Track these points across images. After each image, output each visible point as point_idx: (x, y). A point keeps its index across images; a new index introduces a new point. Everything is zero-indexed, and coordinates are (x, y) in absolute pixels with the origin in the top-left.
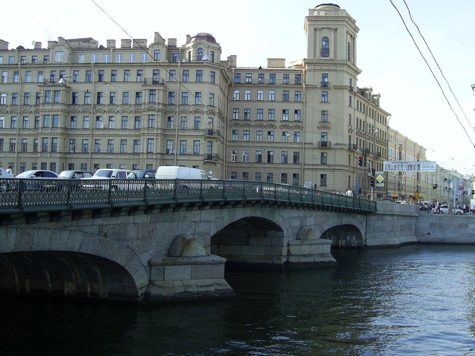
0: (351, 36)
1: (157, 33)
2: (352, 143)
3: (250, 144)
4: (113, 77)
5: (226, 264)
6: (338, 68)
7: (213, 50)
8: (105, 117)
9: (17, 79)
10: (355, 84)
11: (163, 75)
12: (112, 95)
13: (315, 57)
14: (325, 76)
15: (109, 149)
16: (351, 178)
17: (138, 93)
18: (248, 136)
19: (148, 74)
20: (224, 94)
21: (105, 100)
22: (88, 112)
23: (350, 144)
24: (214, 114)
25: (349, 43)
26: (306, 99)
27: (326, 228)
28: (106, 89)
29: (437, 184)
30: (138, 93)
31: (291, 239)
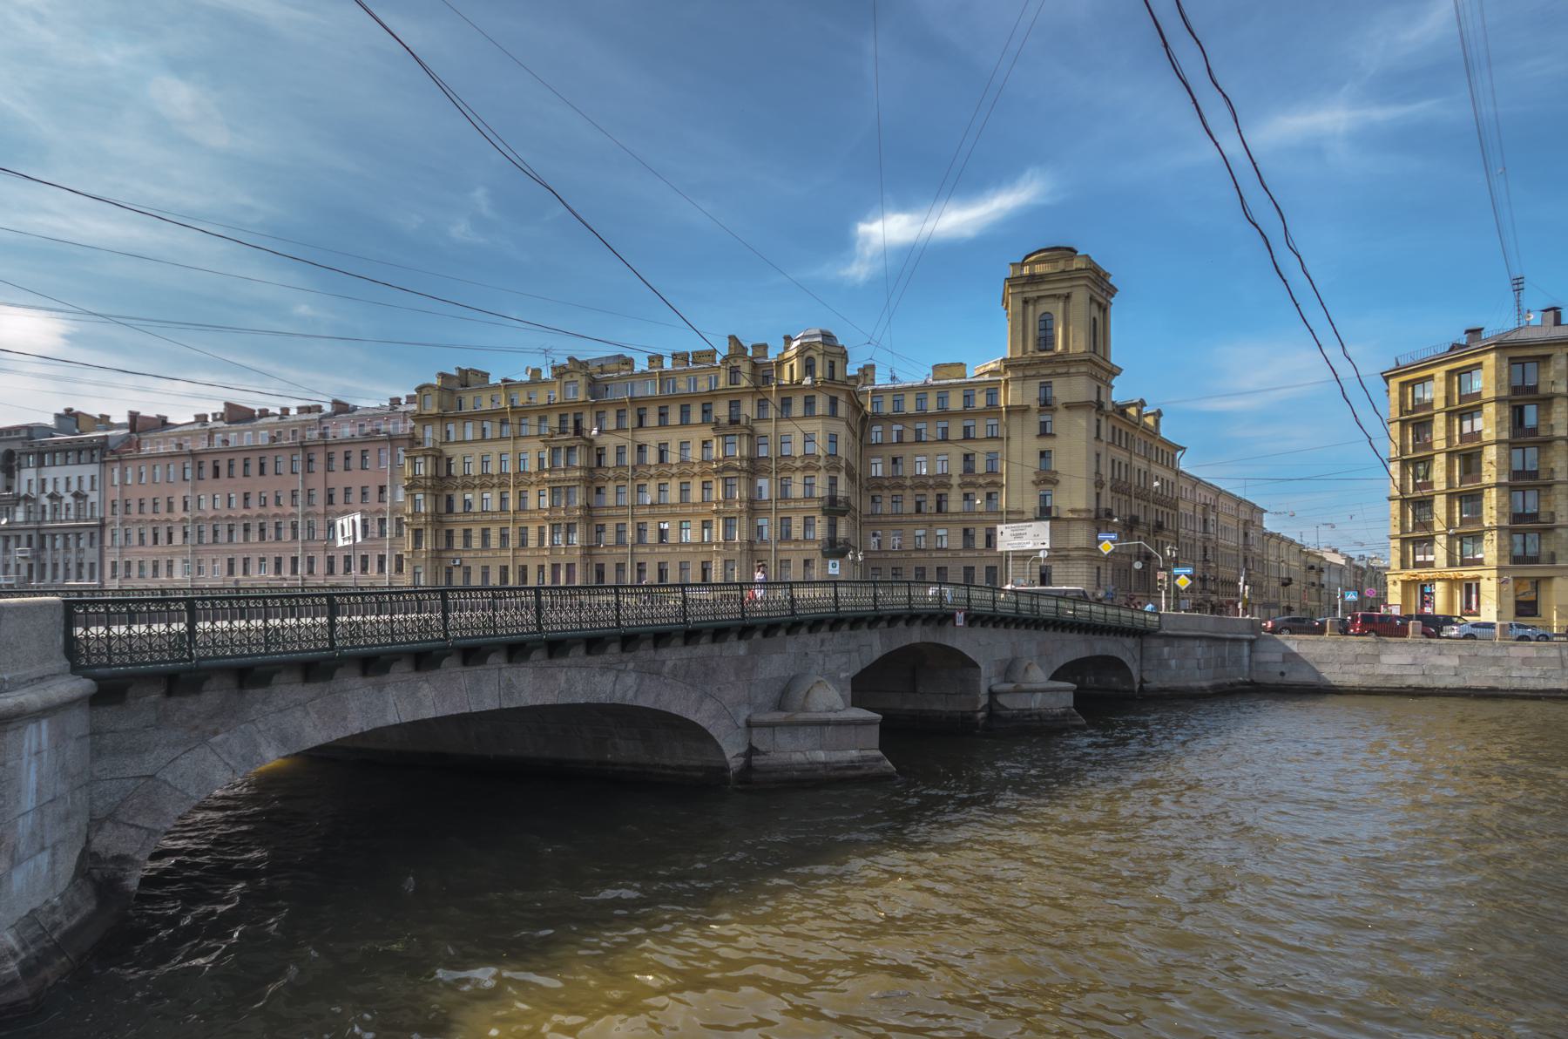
0: (1100, 305)
1: (732, 338)
2: (1103, 505)
3: (904, 519)
4: (706, 415)
5: (881, 724)
6: (1073, 370)
7: (832, 359)
8: (652, 486)
9: (507, 431)
10: (1109, 395)
11: (748, 409)
12: (662, 448)
13: (1024, 351)
14: (1045, 386)
15: (714, 530)
16: (1102, 571)
17: (705, 442)
18: (900, 504)
19: (721, 410)
20: (854, 434)
21: (652, 457)
22: (624, 479)
23: (1098, 509)
24: (838, 470)
25: (1094, 319)
26: (1008, 432)
27: (678, 708)
28: (651, 439)
29: (1291, 576)
30: (705, 442)
31: (994, 681)
